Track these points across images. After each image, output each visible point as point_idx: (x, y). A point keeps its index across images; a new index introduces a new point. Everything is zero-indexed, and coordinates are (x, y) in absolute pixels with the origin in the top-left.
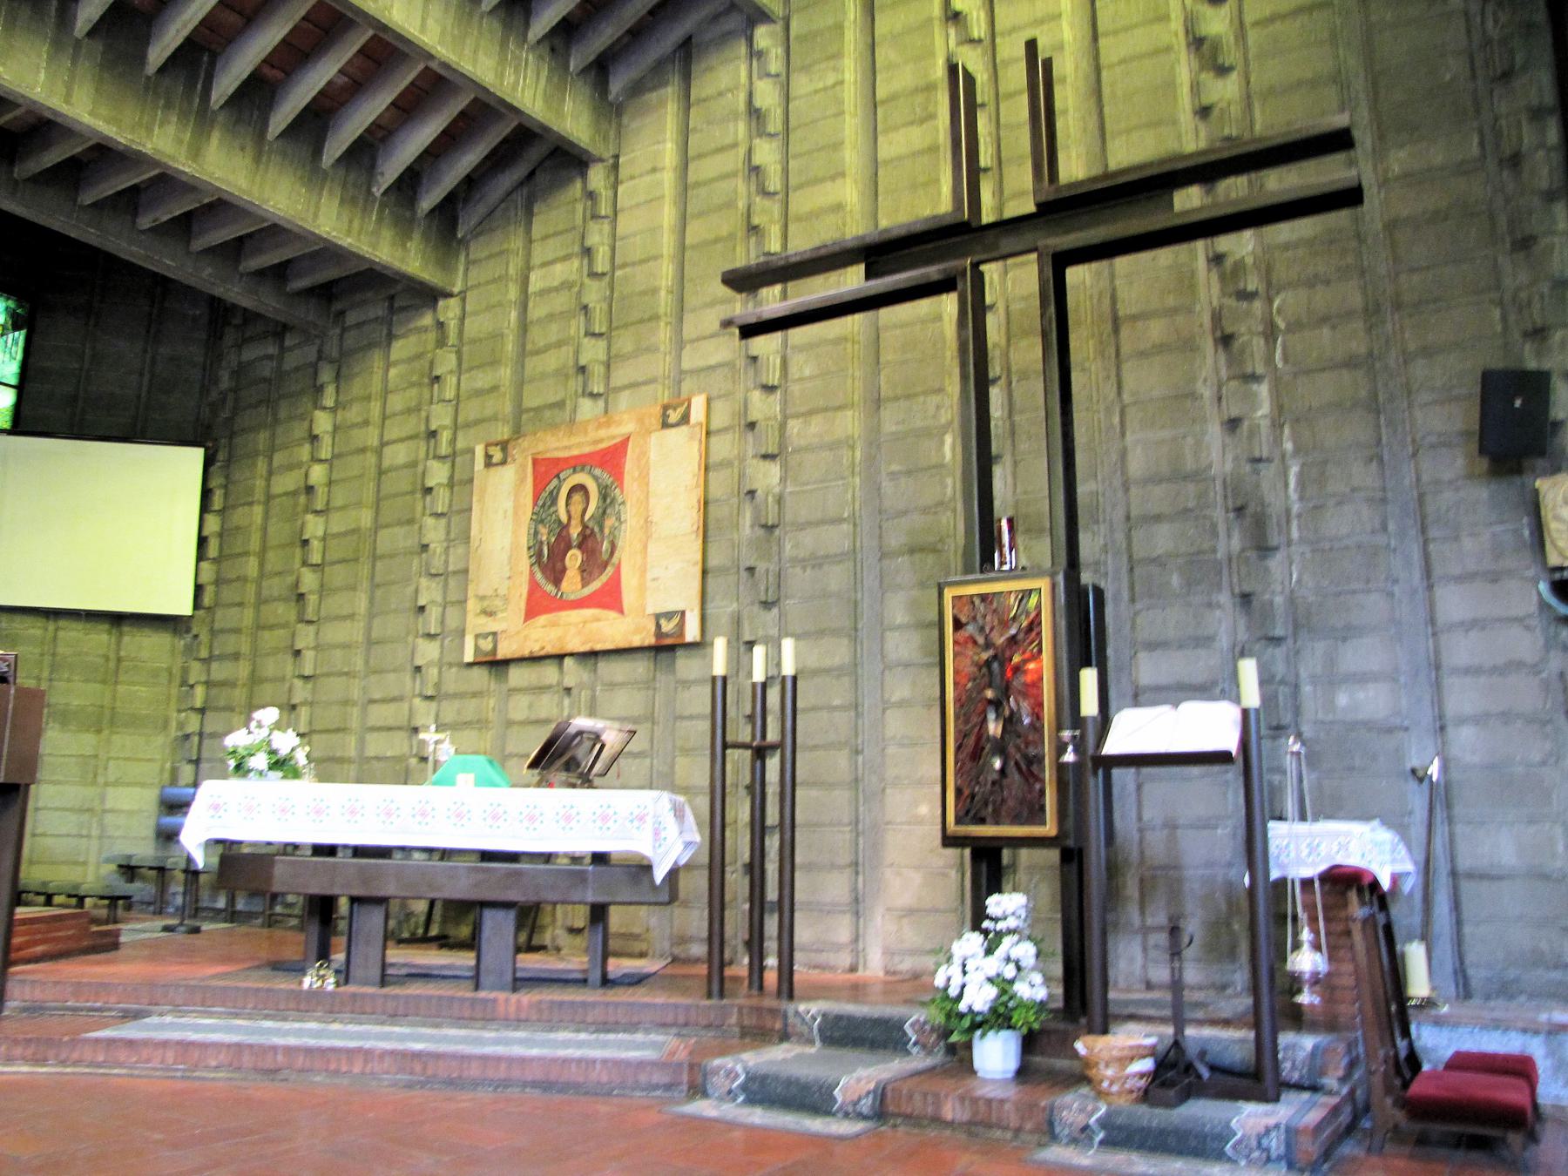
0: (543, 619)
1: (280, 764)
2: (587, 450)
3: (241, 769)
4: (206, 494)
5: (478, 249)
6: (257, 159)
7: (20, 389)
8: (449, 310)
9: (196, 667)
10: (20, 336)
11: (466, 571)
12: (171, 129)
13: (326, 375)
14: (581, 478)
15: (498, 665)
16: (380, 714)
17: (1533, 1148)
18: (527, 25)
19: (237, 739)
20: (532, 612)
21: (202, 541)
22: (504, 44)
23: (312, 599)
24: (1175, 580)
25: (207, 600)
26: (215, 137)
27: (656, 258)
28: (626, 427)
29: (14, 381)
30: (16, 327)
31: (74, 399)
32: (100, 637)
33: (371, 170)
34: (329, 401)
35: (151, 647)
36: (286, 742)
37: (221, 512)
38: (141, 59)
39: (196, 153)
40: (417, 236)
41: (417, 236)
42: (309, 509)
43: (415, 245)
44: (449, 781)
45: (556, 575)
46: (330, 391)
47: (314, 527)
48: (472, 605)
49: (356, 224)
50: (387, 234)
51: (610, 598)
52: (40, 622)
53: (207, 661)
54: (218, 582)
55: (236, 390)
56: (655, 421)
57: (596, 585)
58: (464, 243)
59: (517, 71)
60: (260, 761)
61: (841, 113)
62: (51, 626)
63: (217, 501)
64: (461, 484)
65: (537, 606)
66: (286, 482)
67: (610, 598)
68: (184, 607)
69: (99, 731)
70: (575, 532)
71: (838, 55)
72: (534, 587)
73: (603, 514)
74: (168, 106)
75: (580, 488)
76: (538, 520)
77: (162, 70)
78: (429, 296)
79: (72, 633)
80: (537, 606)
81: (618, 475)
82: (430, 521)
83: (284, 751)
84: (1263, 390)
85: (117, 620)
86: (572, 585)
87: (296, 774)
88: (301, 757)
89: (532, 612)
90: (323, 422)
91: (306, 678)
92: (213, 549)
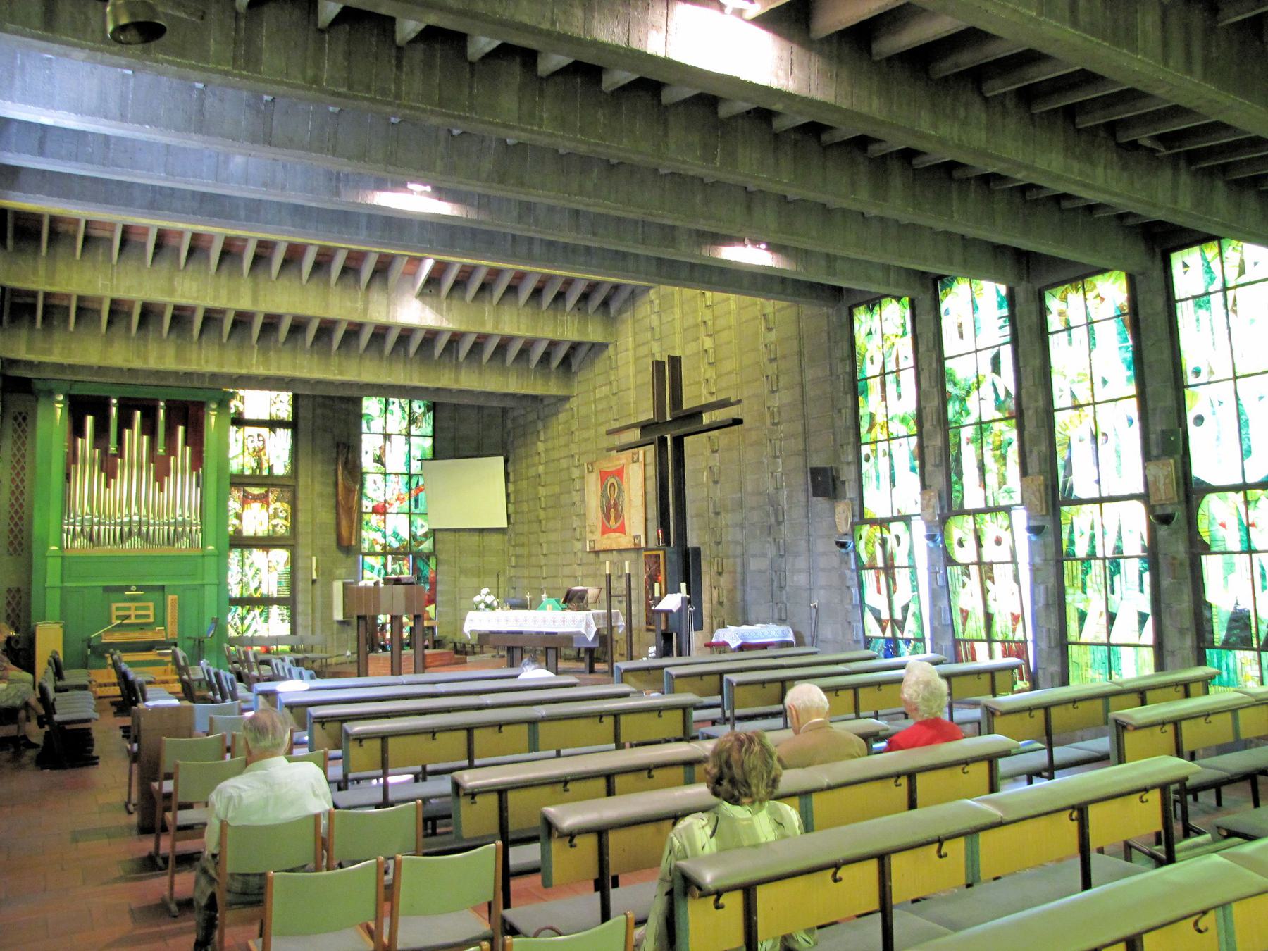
0: (606, 536)
1: (488, 606)
2: (614, 469)
3: (478, 609)
4: (507, 474)
5: (580, 377)
6: (480, 374)
7: (434, 437)
8: (573, 403)
9: (511, 548)
10: (431, 414)
11: (585, 514)
12: (447, 376)
13: (540, 425)
14: (612, 480)
15: (597, 553)
16: (567, 571)
17: (14, 585)
18: (565, 306)
19: (477, 599)
20: (603, 533)
21: (508, 495)
22: (555, 318)
23: (544, 522)
24: (758, 532)
25: (512, 521)
26: (463, 372)
27: (629, 389)
28: (623, 461)
29: (431, 434)
30: (428, 411)
31: (453, 439)
32: (476, 538)
33: (528, 360)
34: (542, 438)
35: (495, 539)
36: (490, 599)
37: (514, 482)
38: (433, 354)
39: (457, 381)
40: (553, 377)
41: (553, 377)
42: (540, 485)
43: (552, 383)
44: (545, 608)
45: (608, 519)
46: (542, 433)
47: (542, 492)
48: (588, 529)
49: (525, 384)
50: (540, 382)
51: (621, 529)
52: (453, 534)
53: (514, 546)
54: (516, 512)
55: (513, 428)
56: (630, 460)
57: (619, 523)
58: (576, 373)
59: (563, 326)
60: (482, 606)
61: (674, 333)
62: (457, 535)
63: (512, 478)
64: (582, 478)
65: (605, 530)
66: (532, 472)
67: (621, 529)
68: (505, 525)
69: (479, 577)
70: (612, 502)
71: (672, 307)
72: (603, 524)
73: (619, 495)
74: (444, 367)
75: (612, 484)
76: (603, 496)
77: (441, 355)
78: (566, 399)
79: (465, 536)
80: (605, 530)
81: (622, 479)
82: (574, 493)
83: (489, 602)
84: (780, 461)
85: (481, 530)
86: (613, 524)
87: (493, 609)
88: (495, 604)
89: (603, 533)
90: (541, 447)
91: (545, 555)
92: (512, 498)
